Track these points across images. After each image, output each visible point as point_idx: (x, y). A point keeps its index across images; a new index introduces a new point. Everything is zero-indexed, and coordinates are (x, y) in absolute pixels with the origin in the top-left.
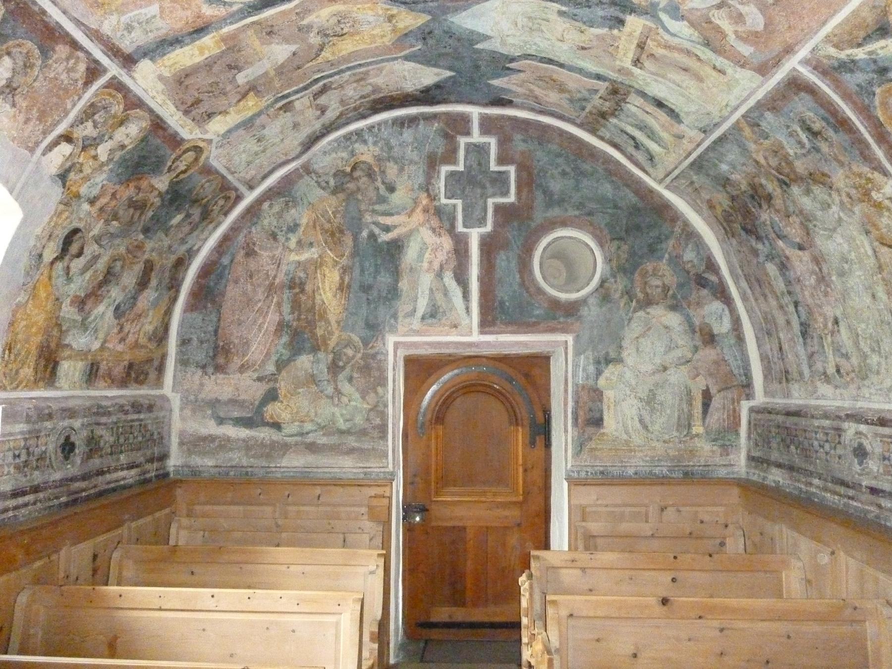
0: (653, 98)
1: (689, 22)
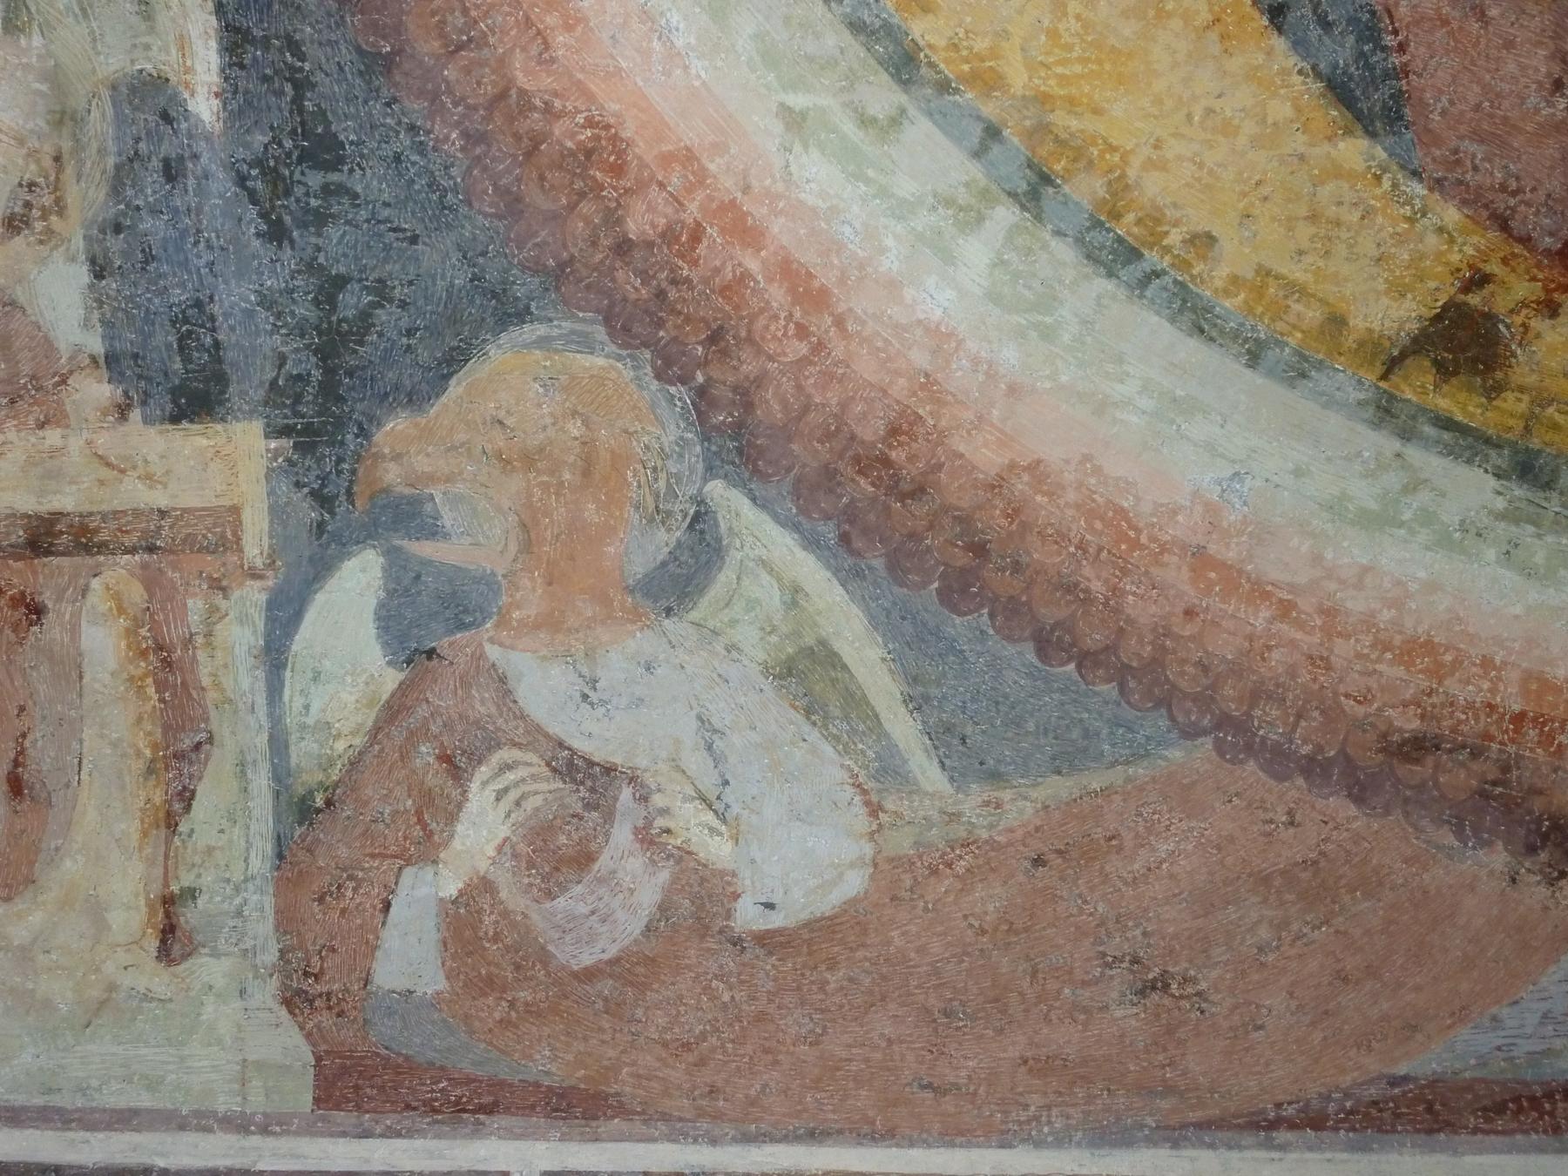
1: (403, 689)
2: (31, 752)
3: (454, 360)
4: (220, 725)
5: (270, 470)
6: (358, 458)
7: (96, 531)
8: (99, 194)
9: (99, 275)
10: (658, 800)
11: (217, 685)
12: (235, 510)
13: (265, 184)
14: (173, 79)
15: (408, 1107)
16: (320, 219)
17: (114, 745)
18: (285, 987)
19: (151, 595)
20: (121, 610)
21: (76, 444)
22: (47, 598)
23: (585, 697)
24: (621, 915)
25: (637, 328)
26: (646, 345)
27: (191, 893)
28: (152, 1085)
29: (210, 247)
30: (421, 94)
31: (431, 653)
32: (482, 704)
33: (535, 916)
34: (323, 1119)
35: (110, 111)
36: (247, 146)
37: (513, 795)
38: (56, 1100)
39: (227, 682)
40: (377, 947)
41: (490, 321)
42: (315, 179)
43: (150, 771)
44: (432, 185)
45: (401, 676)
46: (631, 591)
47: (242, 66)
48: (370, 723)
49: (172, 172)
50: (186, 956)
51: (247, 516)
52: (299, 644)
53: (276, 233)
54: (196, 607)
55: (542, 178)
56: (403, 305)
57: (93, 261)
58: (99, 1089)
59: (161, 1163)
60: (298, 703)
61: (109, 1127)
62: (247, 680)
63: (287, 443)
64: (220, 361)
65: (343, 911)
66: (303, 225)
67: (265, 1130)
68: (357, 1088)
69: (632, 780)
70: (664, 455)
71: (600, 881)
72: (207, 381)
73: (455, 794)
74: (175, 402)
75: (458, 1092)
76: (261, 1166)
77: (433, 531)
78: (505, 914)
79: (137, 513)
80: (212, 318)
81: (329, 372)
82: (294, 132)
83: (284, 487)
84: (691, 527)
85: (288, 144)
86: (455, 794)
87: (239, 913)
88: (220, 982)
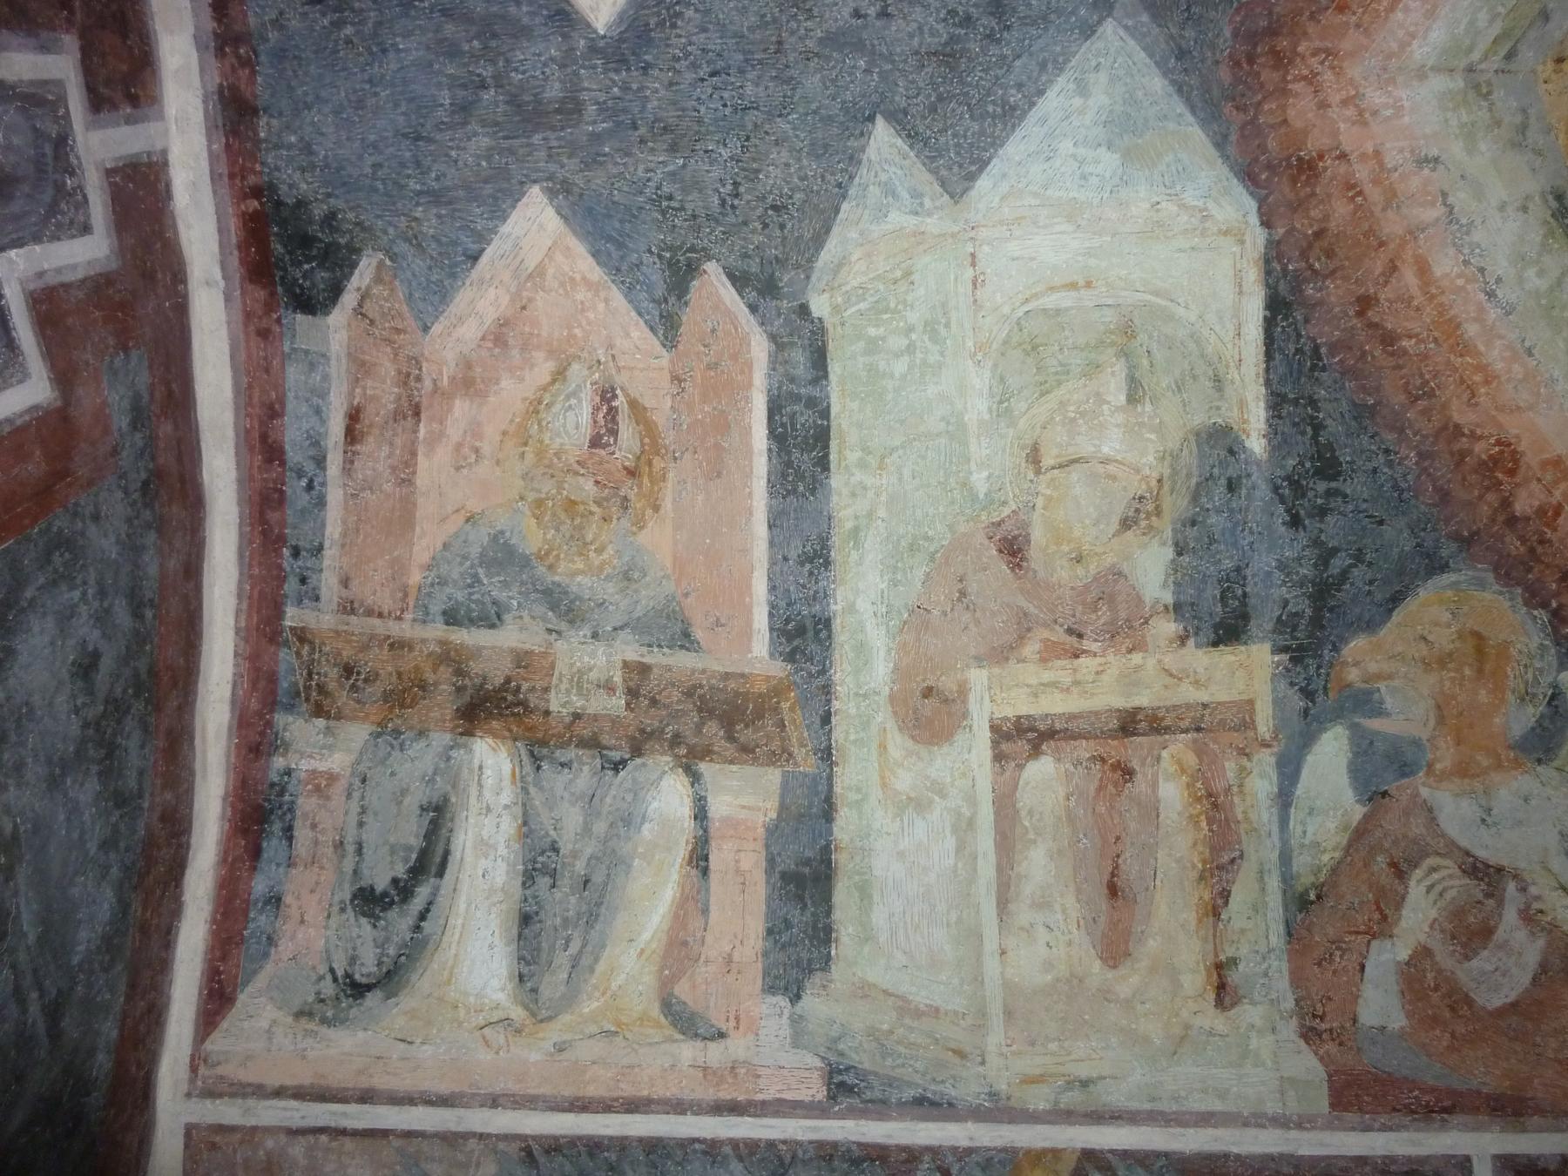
0: (826, 851)
1: (1367, 818)
2: (1123, 867)
3: (1396, 600)
4: (1249, 846)
5: (1274, 675)
6: (1331, 665)
7: (1163, 719)
8: (1183, 502)
9: (1180, 554)
10: (1533, 890)
11: (1247, 819)
12: (1251, 702)
13: (1291, 489)
14: (1236, 427)
15: (1394, 1110)
16: (1322, 512)
17: (1178, 861)
18: (1302, 1026)
19: (1201, 760)
20: (1183, 771)
21: (1151, 663)
22: (1135, 764)
23: (1483, 820)
24: (1514, 970)
25: (1514, 574)
26: (1518, 584)
27: (1233, 962)
28: (1222, 1095)
29: (1252, 533)
30: (1392, 429)
31: (1384, 794)
32: (1417, 828)
33: (1460, 974)
34: (1338, 1119)
35: (1195, 449)
36: (1283, 467)
37: (1439, 888)
38: (1159, 1106)
39: (1253, 816)
40: (1358, 996)
41: (1422, 573)
42: (1322, 486)
43: (1201, 878)
44: (1396, 487)
45: (1365, 810)
46: (1510, 747)
47: (1280, 417)
48: (1345, 842)
49: (1232, 486)
50: (1234, 1005)
51: (1258, 706)
52: (1300, 791)
53: (1295, 522)
54: (1230, 767)
55: (1464, 479)
56: (1370, 564)
57: (1176, 544)
58: (1186, 1098)
59: (1235, 1150)
60: (1299, 829)
61: (1196, 1125)
62: (1265, 815)
63: (1285, 657)
64: (1245, 605)
65: (1334, 972)
66: (1311, 516)
67: (1300, 1126)
68: (1357, 1095)
69: (1515, 877)
70: (1531, 657)
71: (1500, 947)
72: (1236, 618)
73: (1400, 889)
74: (1216, 633)
75: (1427, 1098)
76: (1300, 1153)
77: (1379, 712)
78: (1440, 971)
79: (1188, 706)
80: (1245, 578)
81: (1318, 610)
82: (1312, 458)
83: (1283, 685)
84: (1549, 703)
85: (1308, 465)
86: (1400, 889)
87: (1266, 975)
88: (1258, 1022)
